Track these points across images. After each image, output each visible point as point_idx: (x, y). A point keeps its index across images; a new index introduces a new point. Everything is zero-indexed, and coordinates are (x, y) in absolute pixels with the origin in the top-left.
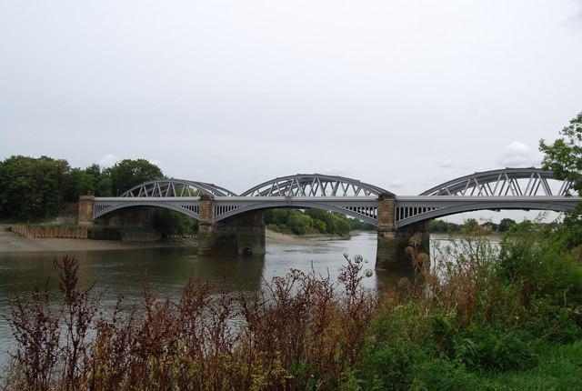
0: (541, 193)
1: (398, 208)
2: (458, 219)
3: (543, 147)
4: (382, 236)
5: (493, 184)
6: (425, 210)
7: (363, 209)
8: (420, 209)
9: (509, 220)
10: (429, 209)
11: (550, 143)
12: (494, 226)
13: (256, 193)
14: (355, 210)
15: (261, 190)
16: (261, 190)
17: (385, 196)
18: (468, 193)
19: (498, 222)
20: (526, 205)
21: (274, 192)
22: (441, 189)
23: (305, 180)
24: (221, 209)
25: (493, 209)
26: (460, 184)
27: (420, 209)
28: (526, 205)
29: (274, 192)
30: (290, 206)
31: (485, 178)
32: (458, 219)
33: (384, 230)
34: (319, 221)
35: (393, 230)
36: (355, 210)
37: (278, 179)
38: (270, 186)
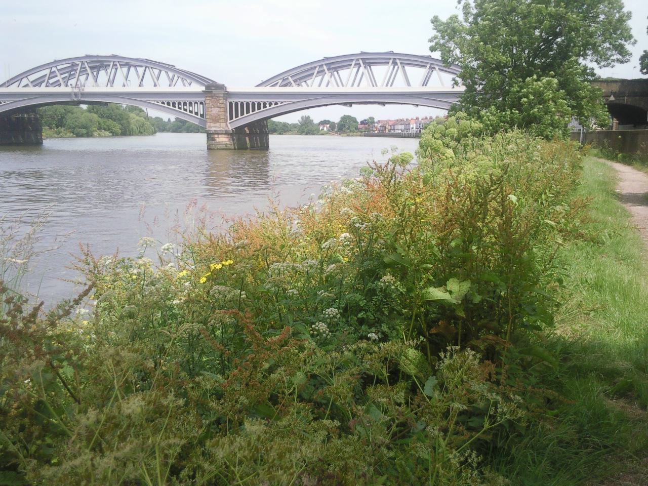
0: (400, 86)
1: (231, 104)
2: (293, 119)
3: (435, 20)
4: (213, 139)
5: (344, 73)
6: (265, 106)
7: (185, 104)
8: (259, 104)
9: (349, 117)
10: (270, 104)
11: (444, 18)
12: (332, 126)
13: (25, 81)
14: (174, 106)
15: (33, 77)
16: (33, 77)
17: (213, 90)
18: (313, 86)
19: (336, 119)
20: (382, 99)
21: (51, 81)
22: (283, 78)
23: (98, 64)
24: (236, 109)
25: (345, 104)
26: (304, 73)
27: (259, 104)
28: (382, 99)
29: (51, 81)
30: (73, 102)
31: (335, 64)
32: (293, 119)
33: (213, 134)
34: (110, 122)
35: (227, 133)
36: (174, 106)
37: (56, 62)
38: (47, 72)
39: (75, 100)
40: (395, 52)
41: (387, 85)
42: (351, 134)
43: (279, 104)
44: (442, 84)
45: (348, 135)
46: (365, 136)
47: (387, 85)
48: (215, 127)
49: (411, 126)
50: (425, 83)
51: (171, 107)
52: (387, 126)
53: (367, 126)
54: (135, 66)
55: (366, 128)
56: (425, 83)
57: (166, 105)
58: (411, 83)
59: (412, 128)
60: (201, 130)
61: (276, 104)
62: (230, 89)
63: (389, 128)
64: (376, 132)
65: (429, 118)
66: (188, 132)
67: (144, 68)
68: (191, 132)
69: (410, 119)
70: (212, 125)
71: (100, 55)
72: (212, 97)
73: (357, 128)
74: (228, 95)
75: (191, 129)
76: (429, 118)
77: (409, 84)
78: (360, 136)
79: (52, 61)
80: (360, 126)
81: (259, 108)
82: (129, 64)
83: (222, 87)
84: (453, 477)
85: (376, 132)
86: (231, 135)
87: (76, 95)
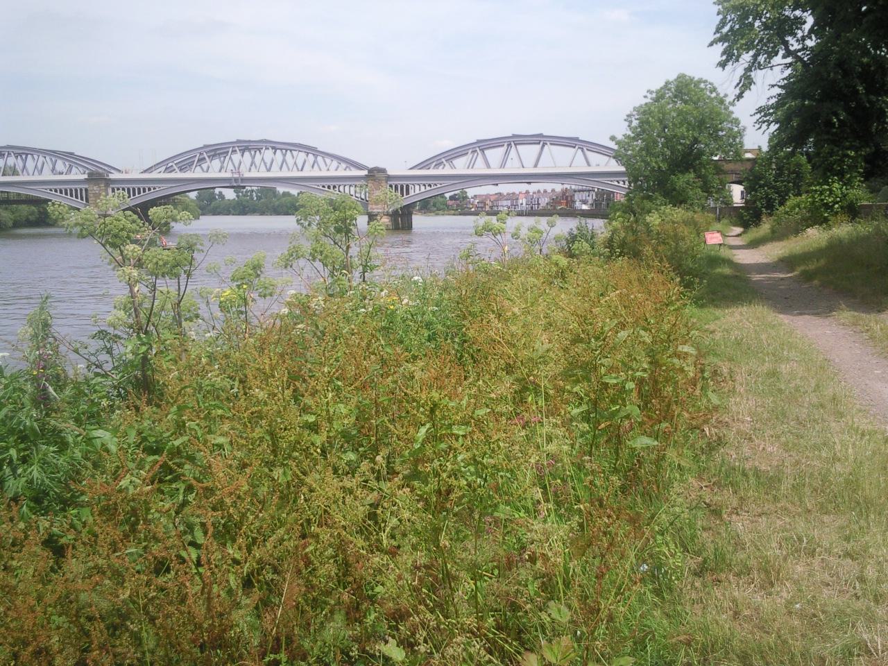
6: (144, 191)
23: (218, 151)
27: (139, 189)
39: (235, 185)
40: (545, 134)
41: (468, 168)
42: (441, 212)
43: (439, 186)
44: (589, 165)
45: (437, 214)
46: (460, 215)
47: (468, 168)
48: (377, 209)
49: (520, 201)
50: (503, 165)
51: (64, 195)
52: (488, 202)
53: (458, 202)
54: (260, 150)
55: (458, 205)
56: (503, 165)
57: (326, 189)
58: (591, 163)
59: (522, 204)
60: (233, 212)
61: (154, 189)
62: (391, 172)
63: (490, 204)
64: (473, 210)
65: (542, 192)
66: (214, 214)
67: (505, 147)
68: (219, 214)
69: (517, 193)
70: (374, 207)
71: (252, 139)
72: (374, 180)
73: (448, 206)
74: (389, 178)
75: (218, 210)
76: (542, 192)
77: (589, 165)
78: (454, 215)
79: (202, 146)
80: (450, 203)
81: (139, 193)
82: (275, 146)
83: (383, 171)
84: (688, 448)
85: (473, 210)
86: (390, 216)
87: (236, 180)
